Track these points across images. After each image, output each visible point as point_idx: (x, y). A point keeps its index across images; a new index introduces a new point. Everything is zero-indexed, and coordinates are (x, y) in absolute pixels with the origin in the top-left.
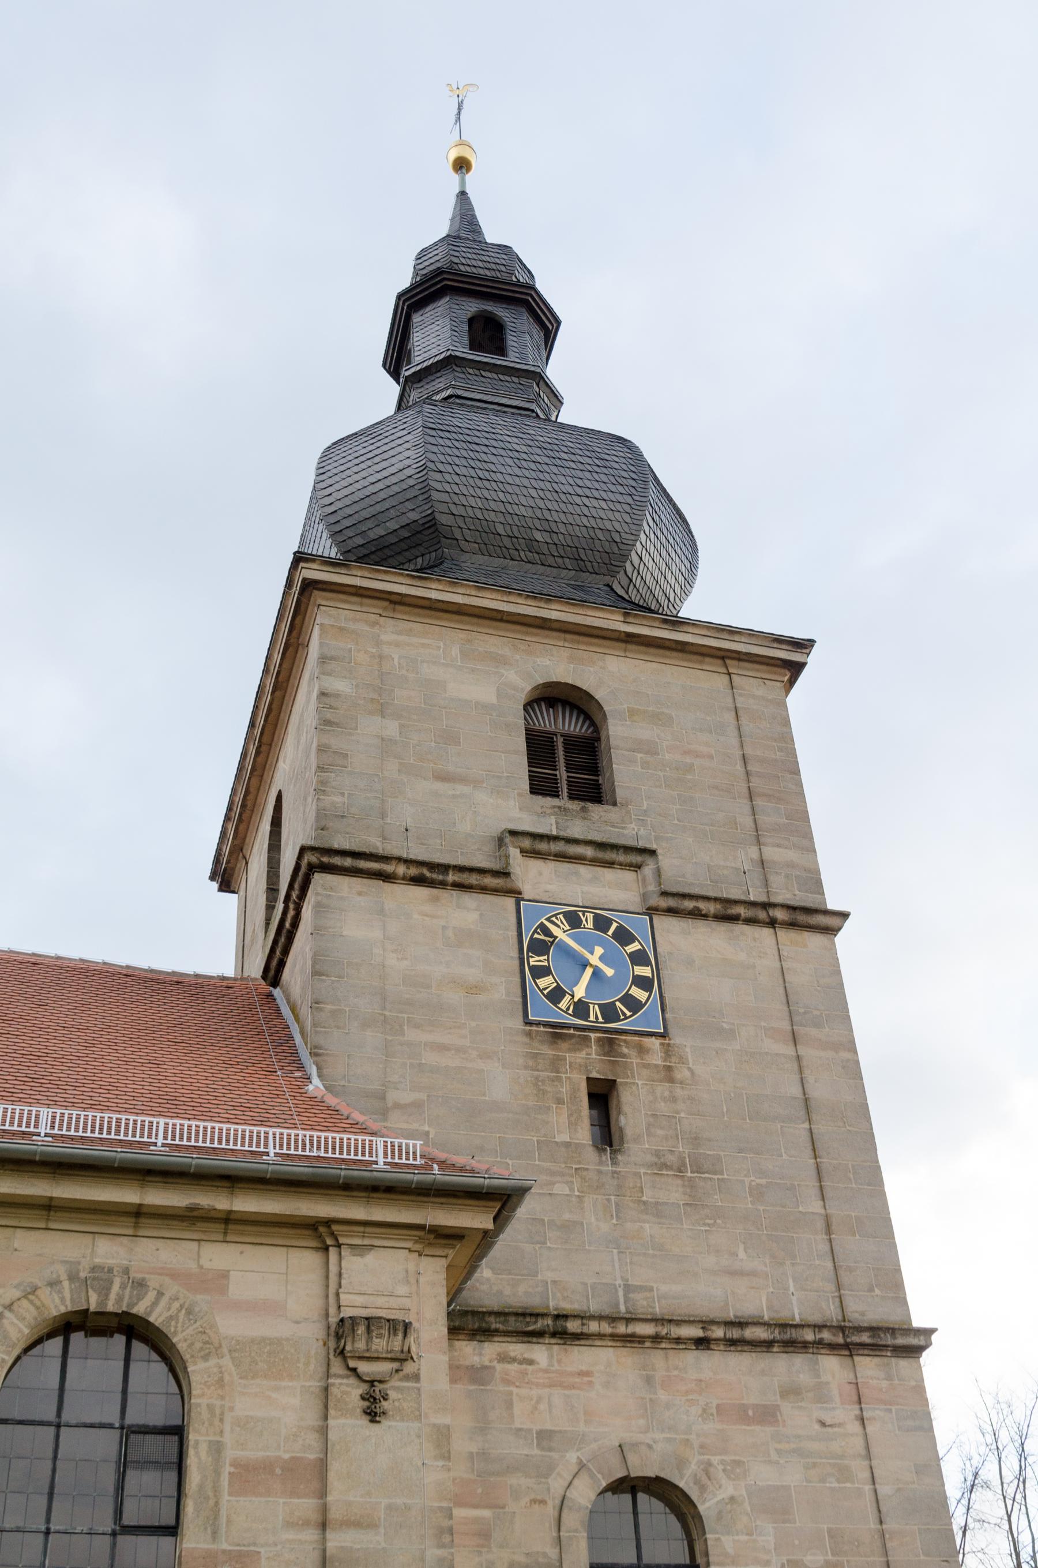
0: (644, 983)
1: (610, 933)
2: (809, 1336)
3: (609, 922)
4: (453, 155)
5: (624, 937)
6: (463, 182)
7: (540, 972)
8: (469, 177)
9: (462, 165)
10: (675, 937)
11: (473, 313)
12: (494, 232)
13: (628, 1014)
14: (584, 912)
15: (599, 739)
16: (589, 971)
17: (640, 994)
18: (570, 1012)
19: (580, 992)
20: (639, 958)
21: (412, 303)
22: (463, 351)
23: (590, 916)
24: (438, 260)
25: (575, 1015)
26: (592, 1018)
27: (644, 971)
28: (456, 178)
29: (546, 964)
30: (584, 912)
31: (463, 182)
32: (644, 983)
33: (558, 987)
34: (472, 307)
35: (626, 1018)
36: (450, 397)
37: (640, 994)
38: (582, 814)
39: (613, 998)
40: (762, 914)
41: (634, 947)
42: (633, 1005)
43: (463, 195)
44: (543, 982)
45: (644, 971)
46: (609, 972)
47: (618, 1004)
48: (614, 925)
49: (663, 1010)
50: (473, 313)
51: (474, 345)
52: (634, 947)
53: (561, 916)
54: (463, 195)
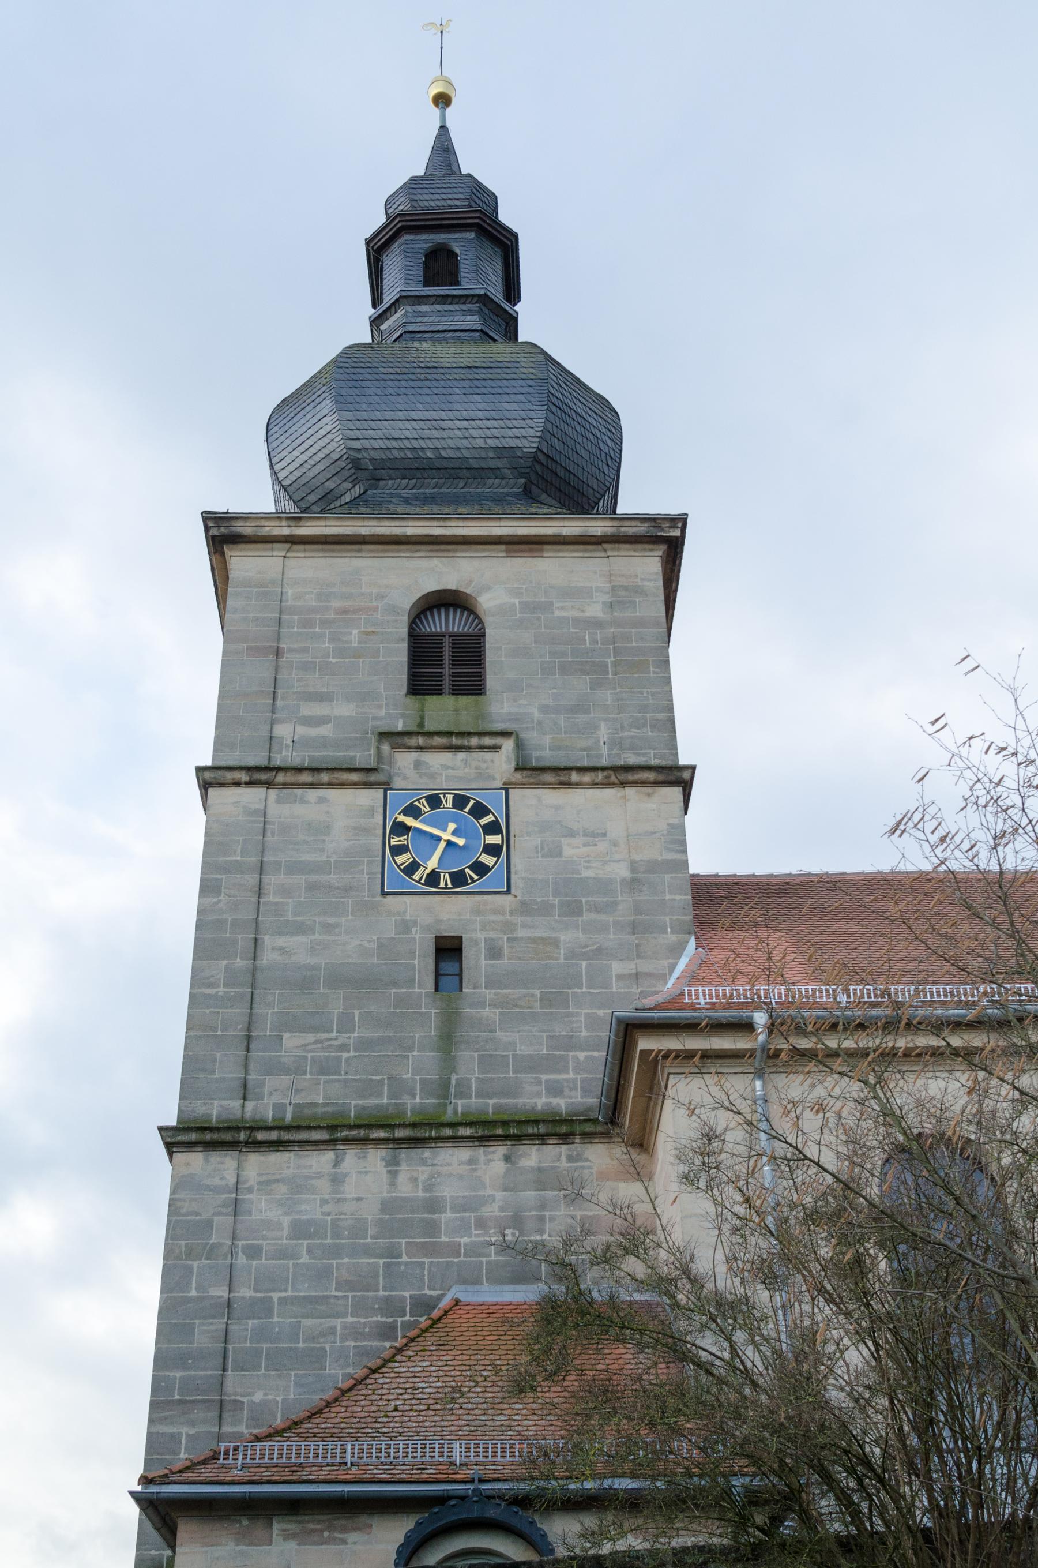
0: (493, 850)
1: (467, 810)
2: (467, 1132)
3: (467, 799)
4: (435, 90)
5: (479, 811)
6: (443, 117)
7: (398, 850)
8: (449, 111)
9: (442, 100)
10: (532, 807)
11: (447, 244)
12: (470, 162)
13: (476, 877)
14: (444, 794)
15: (483, 635)
16: (442, 845)
17: (488, 860)
18: (423, 881)
19: (432, 864)
20: (493, 828)
21: (377, 250)
22: (418, 289)
23: (450, 797)
24: (403, 205)
25: (427, 884)
26: (442, 885)
27: (495, 839)
28: (436, 112)
29: (405, 842)
30: (444, 794)
31: (443, 117)
32: (493, 850)
33: (415, 861)
34: (425, 241)
35: (473, 881)
36: (401, 335)
37: (488, 860)
38: (444, 710)
39: (464, 865)
40: (620, 775)
41: (490, 818)
42: (481, 869)
43: (443, 127)
44: (400, 859)
45: (495, 839)
46: (461, 842)
47: (467, 870)
48: (472, 802)
49: (509, 872)
50: (447, 244)
51: (427, 282)
52: (490, 818)
53: (423, 800)
54: (443, 127)
